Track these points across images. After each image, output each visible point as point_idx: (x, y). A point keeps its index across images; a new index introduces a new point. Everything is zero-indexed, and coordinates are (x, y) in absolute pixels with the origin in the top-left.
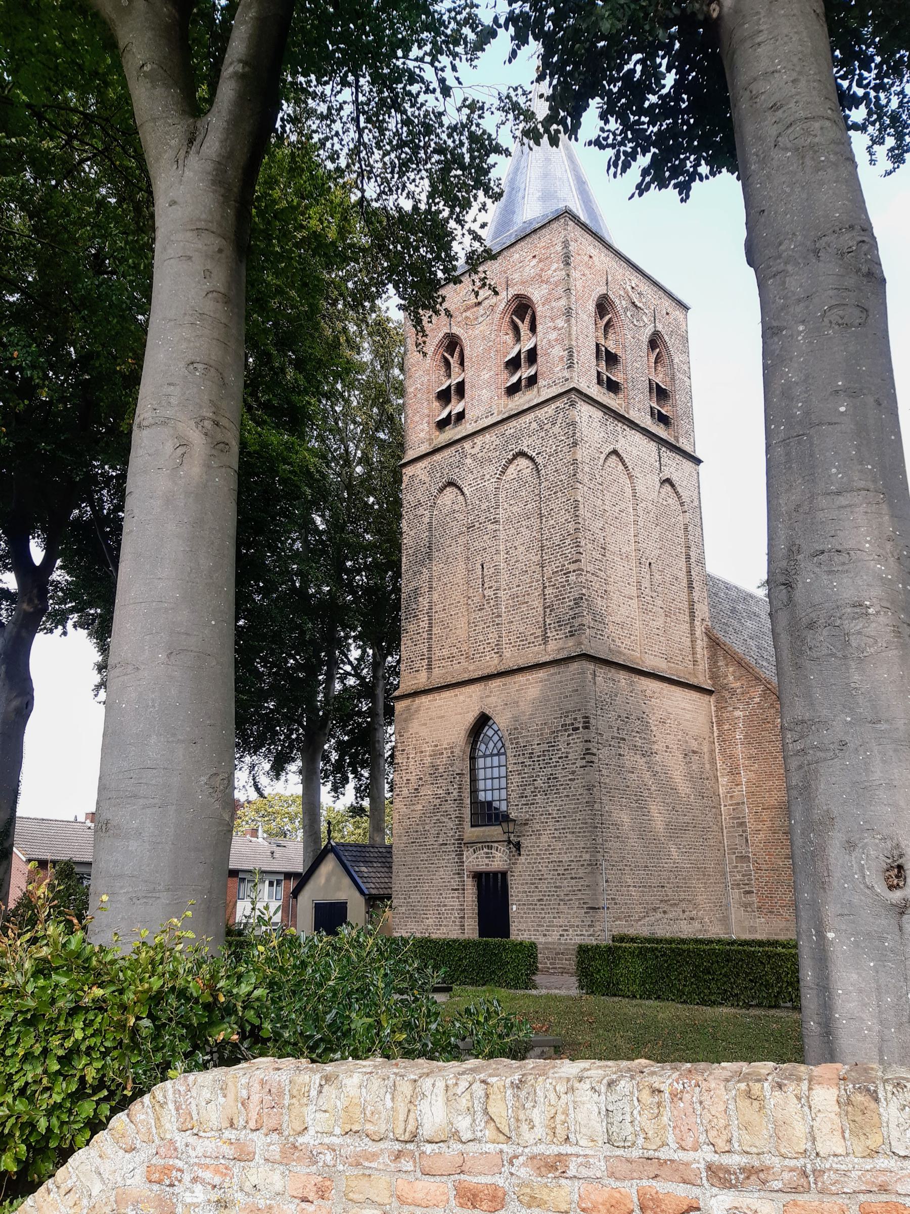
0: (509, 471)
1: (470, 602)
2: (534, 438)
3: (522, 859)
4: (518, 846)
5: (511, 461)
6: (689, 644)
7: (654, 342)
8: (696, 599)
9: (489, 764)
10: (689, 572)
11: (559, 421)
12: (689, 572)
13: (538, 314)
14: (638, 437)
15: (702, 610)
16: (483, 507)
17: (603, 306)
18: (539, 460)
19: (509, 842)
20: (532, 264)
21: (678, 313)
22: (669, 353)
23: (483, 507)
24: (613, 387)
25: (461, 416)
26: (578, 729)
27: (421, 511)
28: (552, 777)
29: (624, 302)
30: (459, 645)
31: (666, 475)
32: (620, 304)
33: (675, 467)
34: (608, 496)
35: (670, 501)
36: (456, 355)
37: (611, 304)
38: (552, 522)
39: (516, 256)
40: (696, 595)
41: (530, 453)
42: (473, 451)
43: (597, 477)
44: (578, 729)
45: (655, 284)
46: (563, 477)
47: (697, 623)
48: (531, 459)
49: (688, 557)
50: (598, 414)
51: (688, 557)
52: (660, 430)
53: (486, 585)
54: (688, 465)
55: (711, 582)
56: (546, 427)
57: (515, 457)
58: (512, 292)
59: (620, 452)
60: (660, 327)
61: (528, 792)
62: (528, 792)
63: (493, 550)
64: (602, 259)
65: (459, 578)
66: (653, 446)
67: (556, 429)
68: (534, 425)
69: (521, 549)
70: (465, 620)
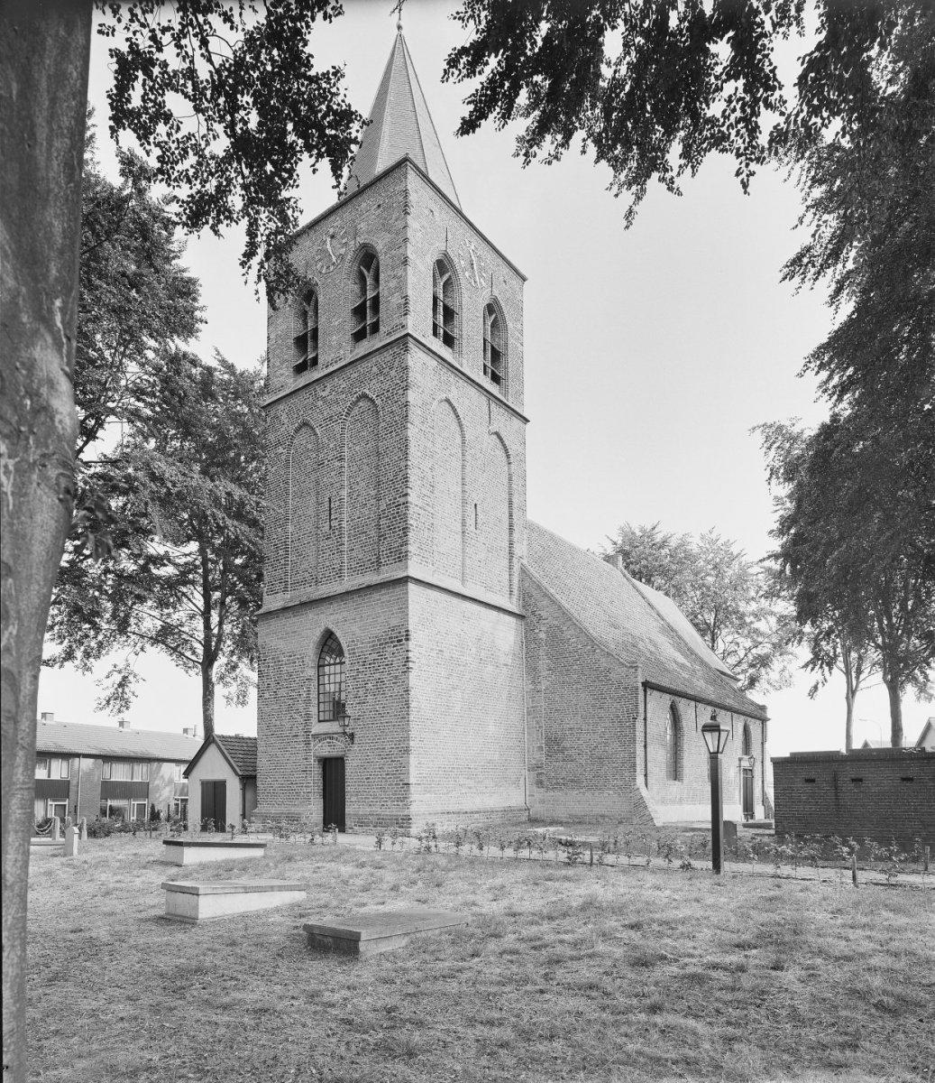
0: (352, 414)
1: (319, 532)
2: (374, 381)
3: (355, 747)
4: (352, 736)
5: (355, 404)
6: (507, 577)
7: (491, 308)
8: (515, 540)
9: (332, 672)
10: (511, 515)
11: (396, 364)
12: (511, 515)
13: (381, 262)
14: (472, 391)
15: (520, 549)
16: (331, 446)
17: (442, 266)
18: (378, 402)
19: (345, 733)
20: (377, 213)
21: (515, 282)
22: (504, 320)
23: (331, 446)
24: (449, 341)
25: (676, 772)
26: (401, 641)
27: (280, 450)
28: (380, 681)
29: (462, 262)
30: (310, 570)
31: (494, 428)
32: (460, 264)
33: (507, 426)
34: (439, 440)
35: (498, 452)
36: (312, 303)
37: (450, 261)
38: (387, 460)
39: (364, 205)
40: (516, 535)
41: (371, 395)
42: (324, 394)
43: (429, 420)
44: (401, 641)
45: (509, 263)
46: (397, 418)
47: (515, 560)
48: (372, 400)
49: (510, 503)
50: (433, 363)
51: (510, 503)
52: (493, 388)
53: (333, 517)
54: (516, 422)
55: (531, 527)
56: (385, 371)
57: (359, 399)
58: (360, 240)
59: (452, 401)
60: (496, 293)
61: (361, 693)
62: (361, 693)
63: (338, 485)
64: (443, 216)
65: (311, 512)
66: (483, 400)
67: (393, 373)
68: (375, 369)
69: (363, 484)
70: (314, 548)
